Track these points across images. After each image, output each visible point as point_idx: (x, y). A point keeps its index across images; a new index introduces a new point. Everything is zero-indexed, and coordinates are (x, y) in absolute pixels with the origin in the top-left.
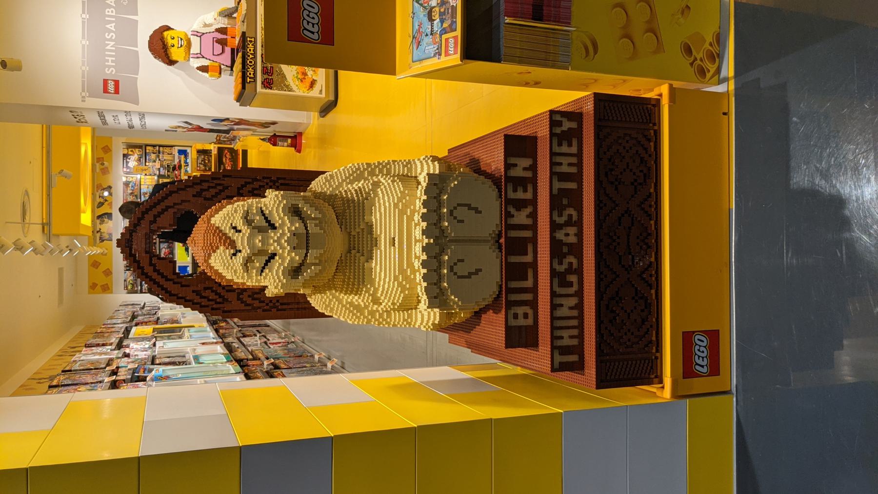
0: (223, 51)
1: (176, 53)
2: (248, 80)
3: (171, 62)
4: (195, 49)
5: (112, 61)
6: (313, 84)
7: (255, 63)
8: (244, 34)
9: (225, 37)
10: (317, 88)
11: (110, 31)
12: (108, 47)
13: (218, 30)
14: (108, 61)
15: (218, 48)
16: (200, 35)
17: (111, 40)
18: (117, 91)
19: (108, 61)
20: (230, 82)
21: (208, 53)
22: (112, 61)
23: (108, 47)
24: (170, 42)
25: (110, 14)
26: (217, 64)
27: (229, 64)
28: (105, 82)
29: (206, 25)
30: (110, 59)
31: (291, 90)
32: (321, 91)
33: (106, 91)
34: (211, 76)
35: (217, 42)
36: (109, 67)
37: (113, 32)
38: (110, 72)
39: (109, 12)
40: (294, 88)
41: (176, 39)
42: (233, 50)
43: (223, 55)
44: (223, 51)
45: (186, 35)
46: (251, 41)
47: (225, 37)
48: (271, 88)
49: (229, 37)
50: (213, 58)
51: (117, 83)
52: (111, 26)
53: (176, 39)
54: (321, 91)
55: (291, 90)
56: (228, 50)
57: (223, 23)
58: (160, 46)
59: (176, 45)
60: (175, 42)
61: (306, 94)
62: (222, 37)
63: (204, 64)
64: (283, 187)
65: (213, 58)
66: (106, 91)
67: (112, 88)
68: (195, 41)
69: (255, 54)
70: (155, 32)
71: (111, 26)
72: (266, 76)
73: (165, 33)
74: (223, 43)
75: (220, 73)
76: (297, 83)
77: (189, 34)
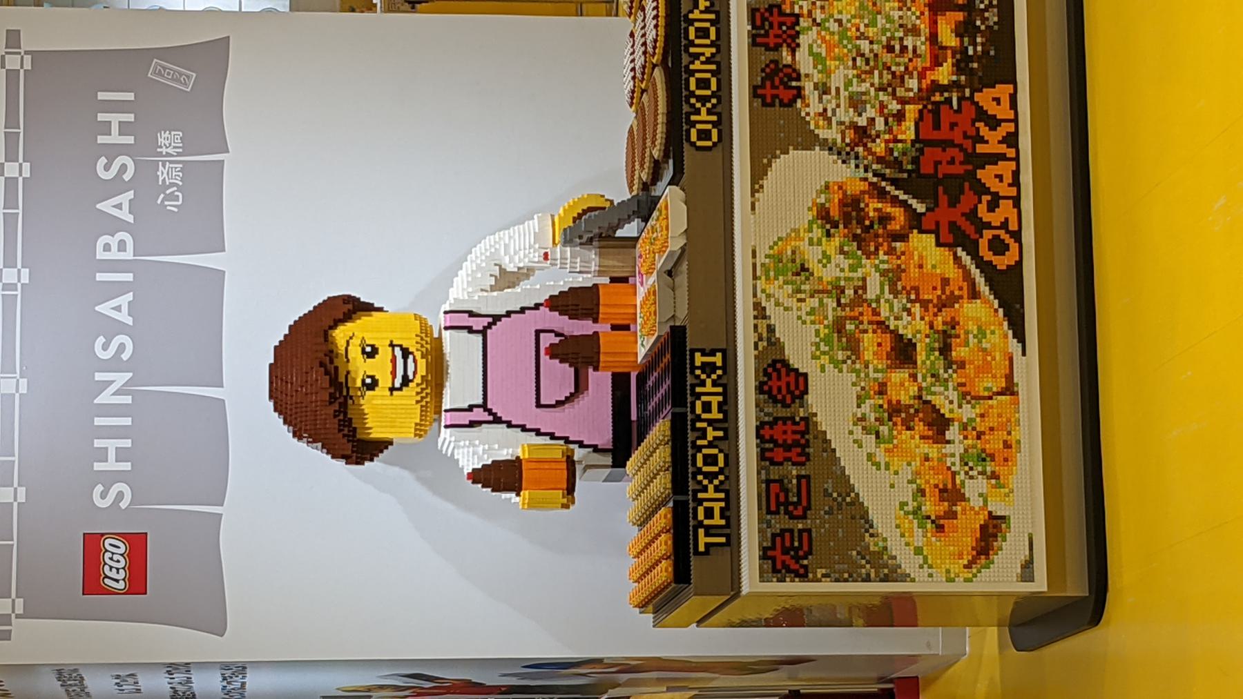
0: (580, 386)
1: (383, 413)
2: (703, 540)
3: (358, 448)
4: (461, 389)
5: (121, 455)
6: (990, 533)
7: (732, 460)
8: (677, 336)
9: (583, 327)
10: (1010, 552)
11: (112, 328)
12: (105, 398)
13: (558, 303)
14: (102, 455)
15: (559, 377)
16: (482, 325)
17: (115, 364)
18: (137, 583)
19: (102, 455)
20: (617, 510)
21: (513, 398)
22: (121, 455)
23: (105, 398)
24: (360, 368)
25: (114, 255)
26: (556, 451)
27: (605, 437)
28: (93, 544)
29: (506, 279)
30: (112, 445)
31: (905, 578)
32: (1028, 565)
33: (93, 583)
34: (533, 504)
35: (553, 352)
36: (110, 478)
37: (121, 328)
38: (113, 502)
39: (110, 247)
40: (907, 562)
41: (385, 354)
42: (620, 382)
43: (583, 402)
44: (580, 386)
45: (425, 329)
46: (709, 368)
47: (583, 327)
48: (803, 575)
49: (603, 328)
50: (546, 420)
51: (137, 544)
52: (118, 309)
53: (385, 354)
54: (1028, 565)
55: (905, 578)
56: (600, 383)
57: (579, 270)
58: (318, 390)
59: (385, 382)
60: (380, 367)
61: (959, 587)
62: (573, 331)
63: (505, 454)
64: (736, 586)
65: (546, 420)
66: (93, 583)
67: (116, 569)
68: (462, 352)
69: (727, 423)
70: (296, 328)
71: (118, 309)
72: (780, 522)
73: (340, 334)
74: (579, 355)
75: (570, 490)
76: (918, 539)
77: (438, 321)
